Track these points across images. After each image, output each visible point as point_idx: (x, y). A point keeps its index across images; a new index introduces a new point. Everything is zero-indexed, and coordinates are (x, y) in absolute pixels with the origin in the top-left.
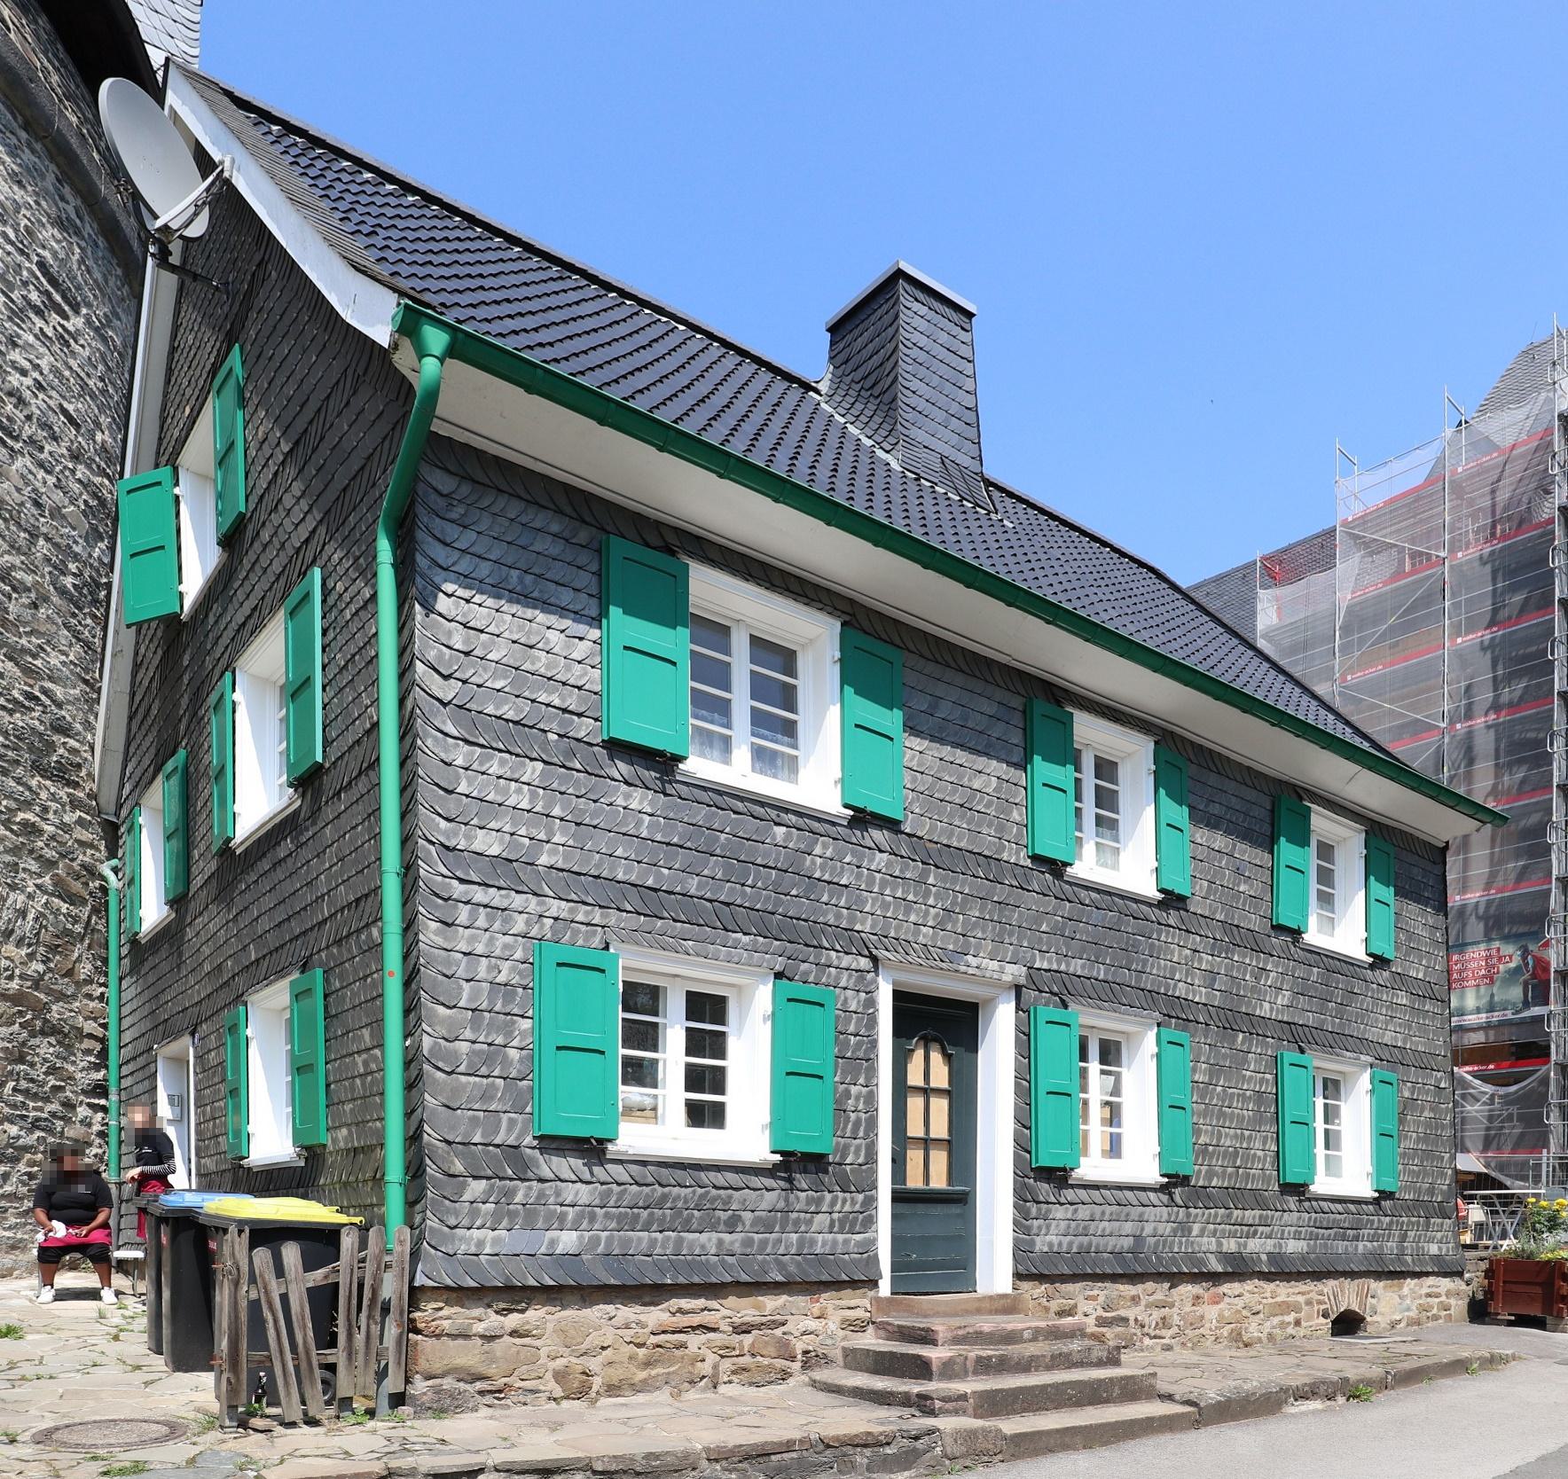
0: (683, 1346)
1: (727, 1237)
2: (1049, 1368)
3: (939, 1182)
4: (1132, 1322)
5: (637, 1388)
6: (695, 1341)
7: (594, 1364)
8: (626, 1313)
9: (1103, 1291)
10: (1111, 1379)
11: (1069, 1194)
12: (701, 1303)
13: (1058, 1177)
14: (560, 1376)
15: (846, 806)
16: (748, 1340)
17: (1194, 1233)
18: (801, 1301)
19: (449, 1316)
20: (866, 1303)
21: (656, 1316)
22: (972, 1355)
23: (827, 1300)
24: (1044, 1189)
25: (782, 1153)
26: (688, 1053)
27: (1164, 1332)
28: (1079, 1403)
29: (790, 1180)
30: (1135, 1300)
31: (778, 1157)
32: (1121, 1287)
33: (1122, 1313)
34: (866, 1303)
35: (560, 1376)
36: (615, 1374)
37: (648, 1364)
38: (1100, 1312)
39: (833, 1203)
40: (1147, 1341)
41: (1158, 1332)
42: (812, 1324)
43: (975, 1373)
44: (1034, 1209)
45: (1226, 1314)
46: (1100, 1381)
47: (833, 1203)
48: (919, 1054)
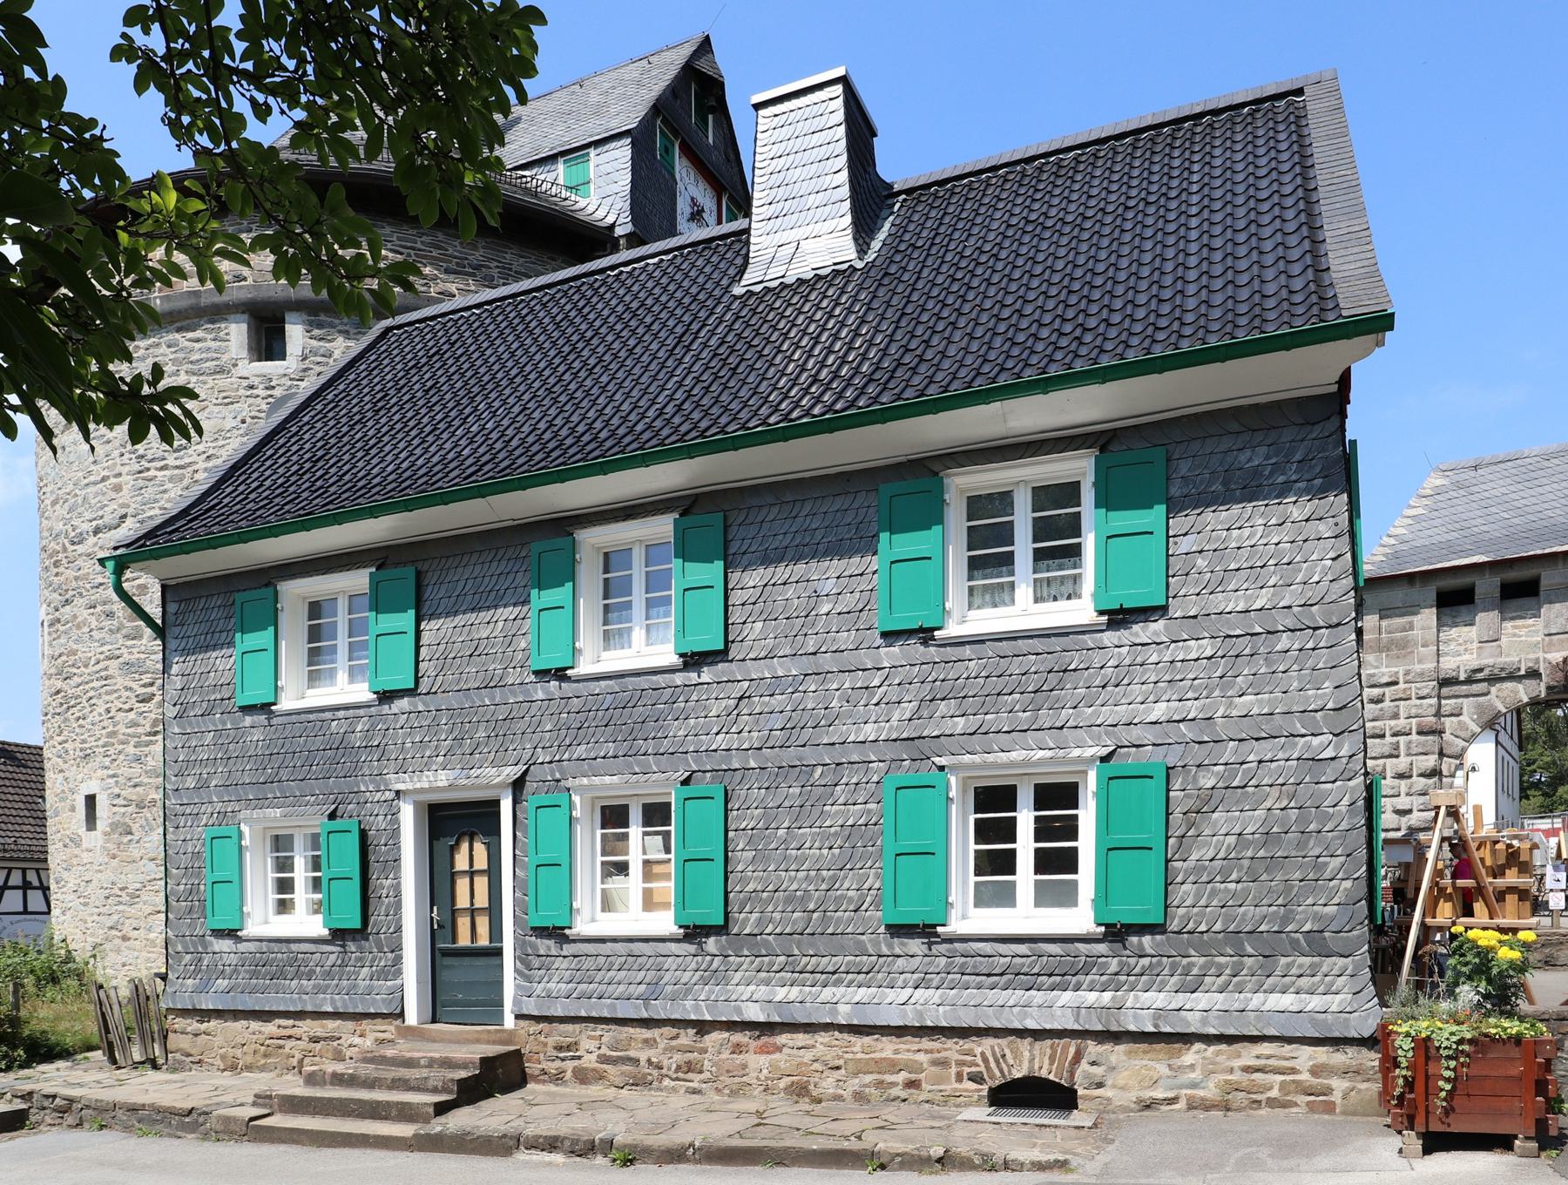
0: (281, 1047)
1: (305, 982)
2: (390, 1088)
3: (483, 941)
4: (643, 1063)
5: (263, 1069)
6: (289, 1044)
7: (238, 1053)
8: (255, 1025)
9: (609, 1034)
10: (388, 1103)
11: (568, 949)
12: (291, 1022)
13: (557, 934)
14: (223, 1057)
15: (1101, 613)
16: (318, 1046)
17: (735, 981)
18: (350, 1025)
19: (179, 1023)
20: (392, 1028)
21: (270, 1028)
22: (330, 1070)
23: (366, 1025)
24: (545, 945)
25: (1107, 926)
26: (1075, 849)
27: (690, 1076)
28: (362, 1116)
29: (343, 946)
30: (647, 1042)
31: (1103, 929)
32: (631, 1030)
33: (632, 1053)
34: (392, 1028)
35: (223, 1057)
36: (249, 1059)
37: (265, 1056)
38: (604, 1050)
39: (373, 960)
40: (666, 1082)
41: (680, 1075)
42: (357, 1040)
43: (332, 1084)
44: (536, 962)
45: (782, 1065)
46: (379, 1103)
47: (373, 960)
48: (465, 846)
